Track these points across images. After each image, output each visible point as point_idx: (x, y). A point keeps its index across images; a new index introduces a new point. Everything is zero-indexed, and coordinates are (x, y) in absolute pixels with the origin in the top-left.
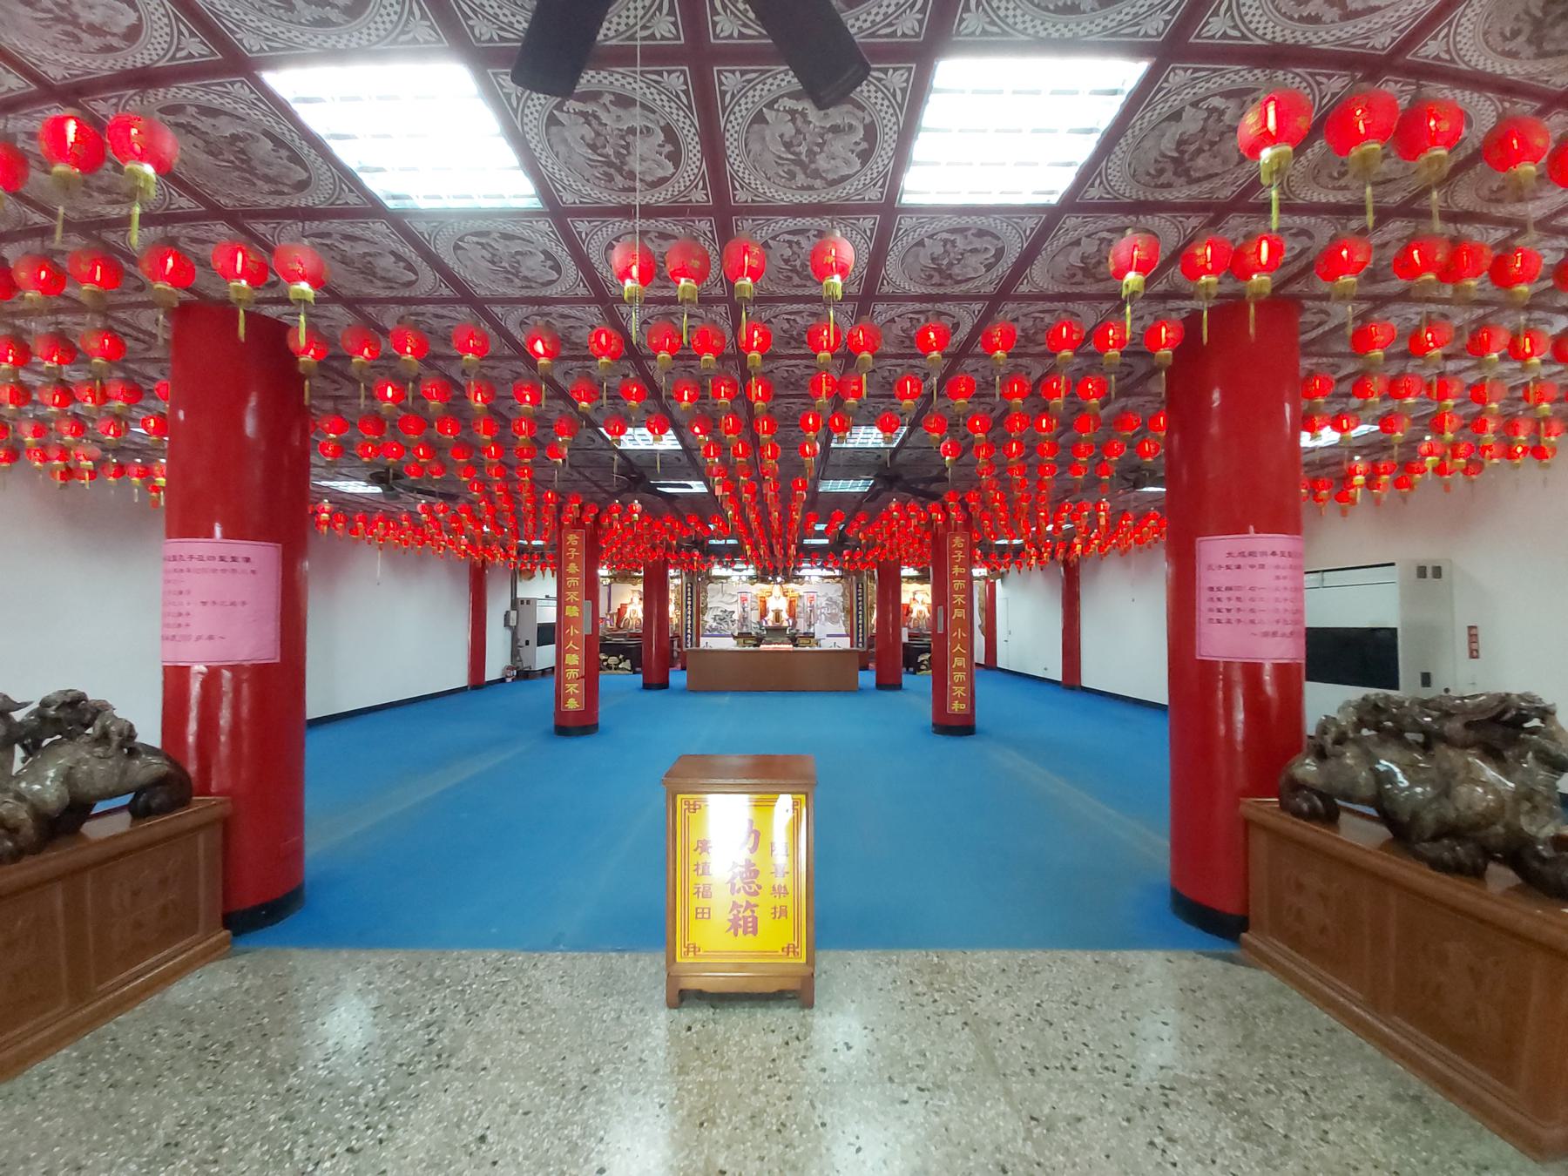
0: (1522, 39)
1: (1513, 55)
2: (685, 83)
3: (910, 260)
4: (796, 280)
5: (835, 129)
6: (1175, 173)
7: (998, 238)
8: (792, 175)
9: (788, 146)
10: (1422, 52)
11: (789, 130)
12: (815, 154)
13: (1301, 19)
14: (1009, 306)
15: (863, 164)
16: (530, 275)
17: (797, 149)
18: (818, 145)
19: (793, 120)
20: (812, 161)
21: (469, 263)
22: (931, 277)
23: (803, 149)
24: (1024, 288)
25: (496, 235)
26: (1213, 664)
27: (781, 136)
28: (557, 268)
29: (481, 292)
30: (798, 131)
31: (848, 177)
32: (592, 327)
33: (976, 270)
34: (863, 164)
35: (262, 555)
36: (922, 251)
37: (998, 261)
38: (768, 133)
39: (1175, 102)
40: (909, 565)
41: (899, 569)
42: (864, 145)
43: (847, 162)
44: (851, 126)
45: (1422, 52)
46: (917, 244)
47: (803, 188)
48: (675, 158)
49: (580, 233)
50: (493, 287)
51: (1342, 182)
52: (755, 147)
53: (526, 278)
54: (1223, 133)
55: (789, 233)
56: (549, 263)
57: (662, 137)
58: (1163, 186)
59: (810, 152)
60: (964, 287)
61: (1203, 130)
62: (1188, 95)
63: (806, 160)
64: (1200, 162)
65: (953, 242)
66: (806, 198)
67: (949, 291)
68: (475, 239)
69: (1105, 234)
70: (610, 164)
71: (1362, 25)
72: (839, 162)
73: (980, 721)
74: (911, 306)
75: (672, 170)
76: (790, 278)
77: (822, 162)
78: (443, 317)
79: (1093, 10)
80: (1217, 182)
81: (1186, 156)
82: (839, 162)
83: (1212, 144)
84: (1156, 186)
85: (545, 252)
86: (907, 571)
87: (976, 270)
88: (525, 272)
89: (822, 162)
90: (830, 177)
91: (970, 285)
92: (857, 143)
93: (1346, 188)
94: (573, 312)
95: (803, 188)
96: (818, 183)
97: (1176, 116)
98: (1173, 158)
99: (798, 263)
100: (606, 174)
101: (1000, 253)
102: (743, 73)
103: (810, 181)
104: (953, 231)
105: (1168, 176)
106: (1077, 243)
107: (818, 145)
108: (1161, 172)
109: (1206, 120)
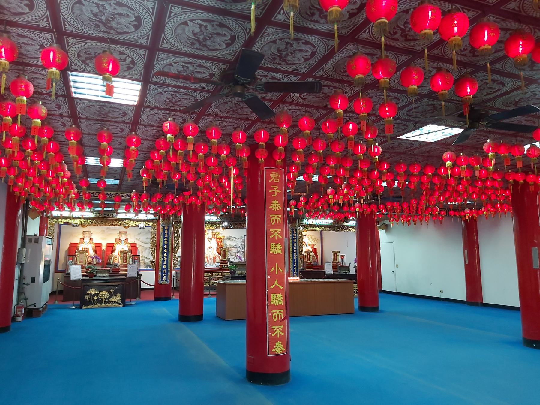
0: (468, 51)
2: (154, 6)
6: (401, 35)
7: (314, 47)
10: (508, 6)
19: (200, 27)
22: (275, 59)
24: (364, 36)
27: (193, 31)
32: (42, 47)
33: (299, 60)
35: (79, 245)
36: (227, 105)
37: (311, 58)
40: (210, 211)
41: (204, 214)
42: (230, 41)
45: (508, 6)
47: (197, 49)
48: (137, 27)
51: (464, 53)
55: (201, 20)
57: (134, 19)
58: (395, 39)
60: (290, 67)
66: (197, 52)
67: (282, 68)
71: (412, 43)
82: (216, 44)
84: (392, 39)
86: (209, 218)
87: (299, 60)
90: (211, 48)
91: (294, 67)
92: (226, 40)
93: (465, 55)
94: (30, 35)
95: (197, 49)
96: (205, 49)
98: (401, 29)
99: (202, 37)
101: (313, 54)
102: (182, 9)
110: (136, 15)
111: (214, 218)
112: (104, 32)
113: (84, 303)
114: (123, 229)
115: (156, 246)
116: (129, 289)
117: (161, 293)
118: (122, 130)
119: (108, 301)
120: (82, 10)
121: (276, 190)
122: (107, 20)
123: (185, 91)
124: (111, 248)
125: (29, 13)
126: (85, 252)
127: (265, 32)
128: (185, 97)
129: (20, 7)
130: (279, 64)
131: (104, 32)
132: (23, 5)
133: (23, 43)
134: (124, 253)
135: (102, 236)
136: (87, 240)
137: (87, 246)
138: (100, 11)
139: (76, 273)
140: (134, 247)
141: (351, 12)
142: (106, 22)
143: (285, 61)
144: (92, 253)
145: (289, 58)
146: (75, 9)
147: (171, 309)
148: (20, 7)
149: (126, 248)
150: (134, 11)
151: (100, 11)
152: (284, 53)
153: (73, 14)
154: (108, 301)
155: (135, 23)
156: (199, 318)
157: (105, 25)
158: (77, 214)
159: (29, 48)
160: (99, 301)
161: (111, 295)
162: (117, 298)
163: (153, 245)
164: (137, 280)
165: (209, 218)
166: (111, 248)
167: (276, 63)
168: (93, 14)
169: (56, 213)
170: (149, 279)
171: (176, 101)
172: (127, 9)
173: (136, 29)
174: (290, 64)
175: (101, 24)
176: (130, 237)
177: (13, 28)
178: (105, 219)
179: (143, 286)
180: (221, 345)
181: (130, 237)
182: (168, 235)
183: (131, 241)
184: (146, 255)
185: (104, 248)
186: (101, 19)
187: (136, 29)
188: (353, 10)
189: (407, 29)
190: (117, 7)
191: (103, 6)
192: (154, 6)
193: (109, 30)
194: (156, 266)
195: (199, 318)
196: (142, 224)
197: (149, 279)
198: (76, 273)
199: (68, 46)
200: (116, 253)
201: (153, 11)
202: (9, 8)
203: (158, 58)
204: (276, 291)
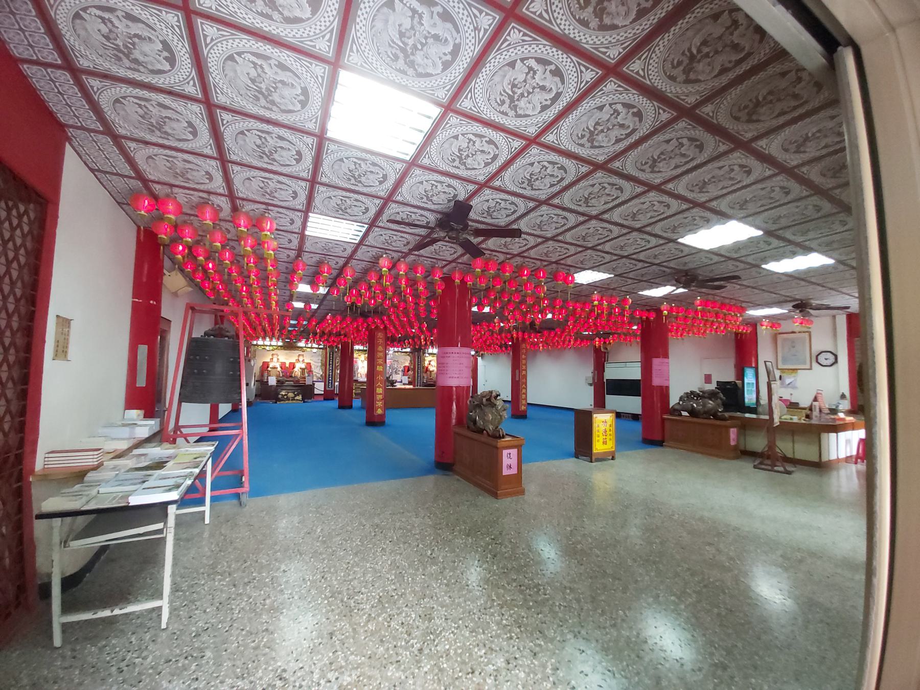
1: (643, 171)
2: (324, 73)
3: (414, 188)
4: (353, 181)
5: (436, 37)
8: (396, 58)
9: (402, 35)
11: (407, 23)
12: (417, 49)
13: (578, 144)
14: (487, 191)
15: (444, 70)
16: (141, 58)
17: (406, 40)
18: (421, 43)
19: (412, 18)
20: (413, 54)
21: (82, 33)
22: (454, 160)
23: (411, 42)
25: (154, 103)
26: (452, 387)
27: (400, 25)
28: (172, 60)
29: (84, 63)
30: (412, 28)
31: (431, 75)
34: (444, 70)
38: (392, 18)
39: (532, 159)
42: (449, 58)
43: (434, 65)
44: (446, 40)
46: (453, 137)
49: (205, 36)
50: (100, 61)
52: (379, 25)
53: (136, 61)
54: (614, 125)
56: (166, 54)
57: (300, 91)
59: (415, 47)
61: (608, 120)
62: (537, 158)
63: (410, 51)
64: (537, 183)
65: (474, 142)
68: (98, 13)
69: (546, 164)
70: (261, 92)
72: (429, 62)
73: (387, 420)
74: (409, 209)
75: (308, 15)
76: (350, 180)
77: (419, 58)
78: (166, 107)
79: (594, 29)
80: (541, 192)
81: (596, 132)
82: (429, 62)
83: (608, 129)
85: (165, 44)
88: (137, 54)
89: (419, 58)
90: (420, 70)
91: (473, 172)
92: (445, 54)
97: (532, 164)
99: (357, 174)
100: (255, 96)
101: (495, 158)
103: (406, 68)
104: (476, 135)
105: (524, 185)
106: (488, 201)
107: (421, 43)
108: (523, 183)
109: (612, 115)
110: (303, 85)
111: (361, 348)
112: (264, 107)
113: (277, 400)
114: (301, 353)
115: (324, 365)
116: (306, 391)
117: (328, 396)
118: (290, 241)
119: (293, 399)
120: (235, 71)
121: (381, 341)
122: (268, 89)
123: (356, 196)
124: (293, 366)
125: (170, 71)
126: (275, 368)
127: (447, 123)
128: (356, 203)
129: (159, 62)
130: (458, 168)
131: (264, 107)
132: (161, 58)
133: (166, 117)
134: (303, 370)
135: (286, 357)
136: (275, 360)
137: (275, 364)
138: (259, 75)
139: (272, 381)
140: (309, 365)
141: (545, 103)
142: (266, 93)
143: (464, 164)
144: (279, 369)
145: (469, 161)
146: (227, 68)
147: (334, 404)
148: (159, 62)
149: (303, 366)
150: (300, 79)
151: (259, 75)
152: (465, 154)
153: (226, 76)
154: (293, 399)
155: (302, 98)
156: (351, 407)
157: (266, 97)
158: (274, 342)
159: (175, 125)
160: (288, 399)
161: (296, 396)
162: (300, 397)
163: (322, 365)
164: (312, 387)
165: (356, 347)
166: (293, 366)
167: (502, 113)
168: (250, 79)
169: (255, 342)
170: (319, 388)
171: (346, 209)
172: (291, 74)
173: (303, 107)
174: (469, 169)
175: (260, 96)
176: (307, 359)
177: (152, 94)
178: (290, 346)
179: (316, 392)
180: (357, 415)
181: (307, 359)
182: (332, 359)
183: (306, 361)
184: (318, 371)
185: (287, 365)
186: (260, 88)
187: (303, 107)
188: (546, 100)
189: (596, 132)
190: (279, 71)
191: (261, 66)
192: (324, 73)
193: (270, 106)
194: (324, 379)
195: (351, 407)
196: (315, 350)
197: (319, 388)
198: (272, 381)
199: (223, 125)
200: (296, 369)
201: (323, 81)
202: (146, 63)
203: (328, 149)
204: (379, 387)
